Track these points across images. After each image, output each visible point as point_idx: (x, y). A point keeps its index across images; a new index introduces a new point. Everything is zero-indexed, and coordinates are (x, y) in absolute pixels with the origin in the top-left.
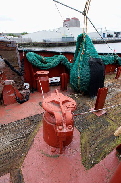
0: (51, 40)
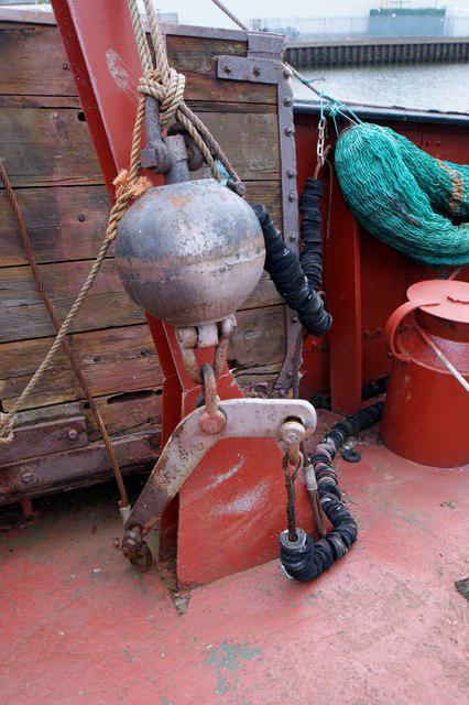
0: (297, 28)
